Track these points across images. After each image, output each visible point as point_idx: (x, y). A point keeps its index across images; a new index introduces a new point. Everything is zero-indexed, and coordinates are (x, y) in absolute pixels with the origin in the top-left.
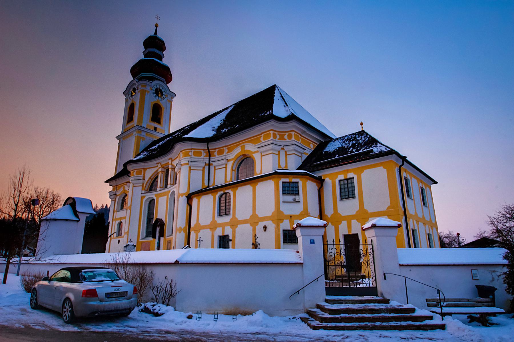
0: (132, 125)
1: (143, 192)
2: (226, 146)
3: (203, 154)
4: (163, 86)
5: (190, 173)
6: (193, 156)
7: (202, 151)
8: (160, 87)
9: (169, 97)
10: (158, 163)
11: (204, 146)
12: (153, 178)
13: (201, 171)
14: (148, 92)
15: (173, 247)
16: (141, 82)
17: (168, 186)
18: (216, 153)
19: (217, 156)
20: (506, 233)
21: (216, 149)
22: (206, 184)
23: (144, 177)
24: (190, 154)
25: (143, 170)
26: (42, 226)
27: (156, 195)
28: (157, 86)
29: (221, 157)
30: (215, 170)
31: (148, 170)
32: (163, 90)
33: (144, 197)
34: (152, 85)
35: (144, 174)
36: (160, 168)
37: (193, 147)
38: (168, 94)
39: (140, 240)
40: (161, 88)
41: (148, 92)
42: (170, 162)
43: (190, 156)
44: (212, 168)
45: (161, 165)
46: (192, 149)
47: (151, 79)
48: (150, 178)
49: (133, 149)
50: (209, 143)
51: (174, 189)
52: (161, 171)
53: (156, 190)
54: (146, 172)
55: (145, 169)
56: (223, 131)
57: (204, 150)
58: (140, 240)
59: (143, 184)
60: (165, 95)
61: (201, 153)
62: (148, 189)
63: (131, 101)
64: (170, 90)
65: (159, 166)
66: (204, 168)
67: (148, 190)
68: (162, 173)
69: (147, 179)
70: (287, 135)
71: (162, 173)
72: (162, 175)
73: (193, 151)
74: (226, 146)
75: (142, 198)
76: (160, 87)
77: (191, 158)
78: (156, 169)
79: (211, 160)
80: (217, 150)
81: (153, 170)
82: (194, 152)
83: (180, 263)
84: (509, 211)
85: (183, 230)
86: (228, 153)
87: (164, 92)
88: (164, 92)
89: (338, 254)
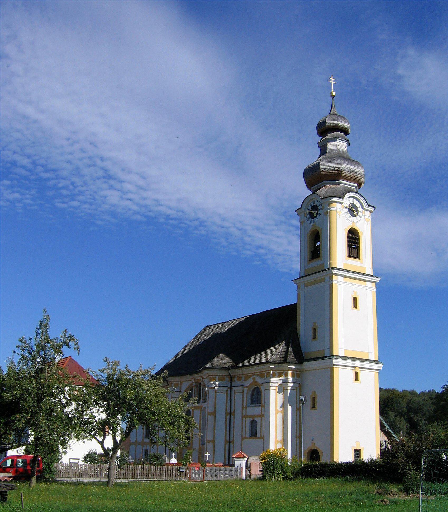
3: (226, 379)
10: (192, 378)
11: (226, 372)
13: (225, 394)
17: (201, 401)
20: (379, 479)
26: (319, 206)
30: (235, 393)
31: (184, 382)
35: (181, 387)
42: (202, 380)
51: (205, 405)
52: (195, 386)
55: (181, 382)
56: (112, 427)
57: (227, 375)
63: (311, 227)
65: (193, 380)
66: (227, 391)
70: (284, 373)
71: (196, 387)
81: (188, 384)
84: (279, 474)
85: (279, 442)
86: (244, 380)
89: (211, 509)
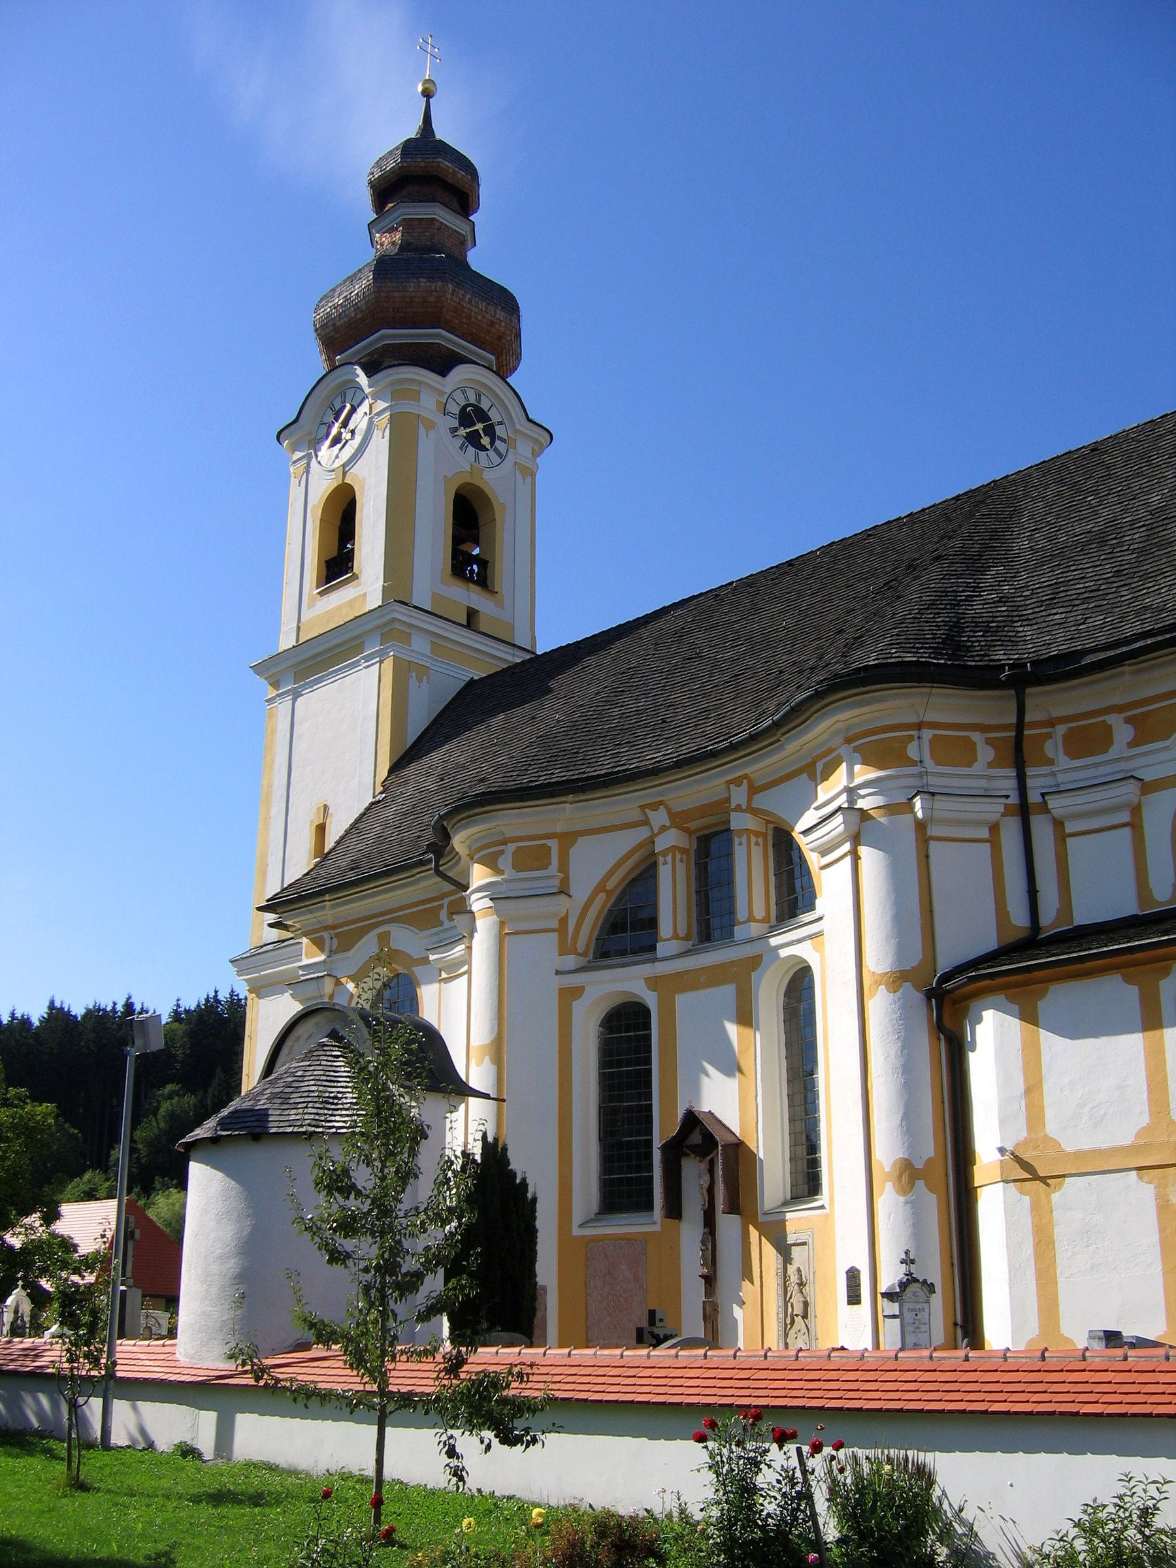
0: (351, 603)
1: (571, 961)
2: (1119, 709)
4: (496, 395)
5: (927, 856)
6: (929, 764)
7: (976, 737)
8: (478, 395)
9: (523, 449)
12: (616, 887)
14: (431, 426)
15: (853, 1276)
16: (389, 376)
18: (1053, 748)
19: (1064, 762)
21: (1052, 723)
22: (1019, 917)
23: (565, 881)
24: (912, 751)
25: (553, 844)
27: (653, 983)
28: (464, 392)
29: (1097, 765)
30: (1061, 837)
31: (581, 840)
32: (495, 416)
33: (578, 991)
34: (448, 391)
35: (564, 867)
36: (663, 829)
37: (930, 717)
38: (516, 431)
39: (576, 1232)
40: (485, 405)
41: (431, 426)
43: (913, 763)
44: (1042, 830)
45: (672, 816)
46: (919, 726)
47: (442, 362)
48: (600, 888)
49: (810, 735)
50: (1029, 690)
53: (653, 948)
54: (573, 851)
55: (568, 839)
58: (576, 1232)
59: (564, 921)
60: (504, 441)
61: (971, 746)
62: (588, 946)
64: (531, 417)
65: (659, 818)
67: (591, 957)
68: (678, 856)
69: (582, 889)
71: (678, 856)
72: (681, 869)
73: (927, 734)
74: (1119, 709)
75: (569, 995)
76: (478, 395)
77: (920, 775)
78: (643, 833)
79: (1030, 783)
80: (1061, 729)
81: (624, 843)
82: (934, 740)
83: (662, 1337)
87: (500, 423)
88: (500, 423)
